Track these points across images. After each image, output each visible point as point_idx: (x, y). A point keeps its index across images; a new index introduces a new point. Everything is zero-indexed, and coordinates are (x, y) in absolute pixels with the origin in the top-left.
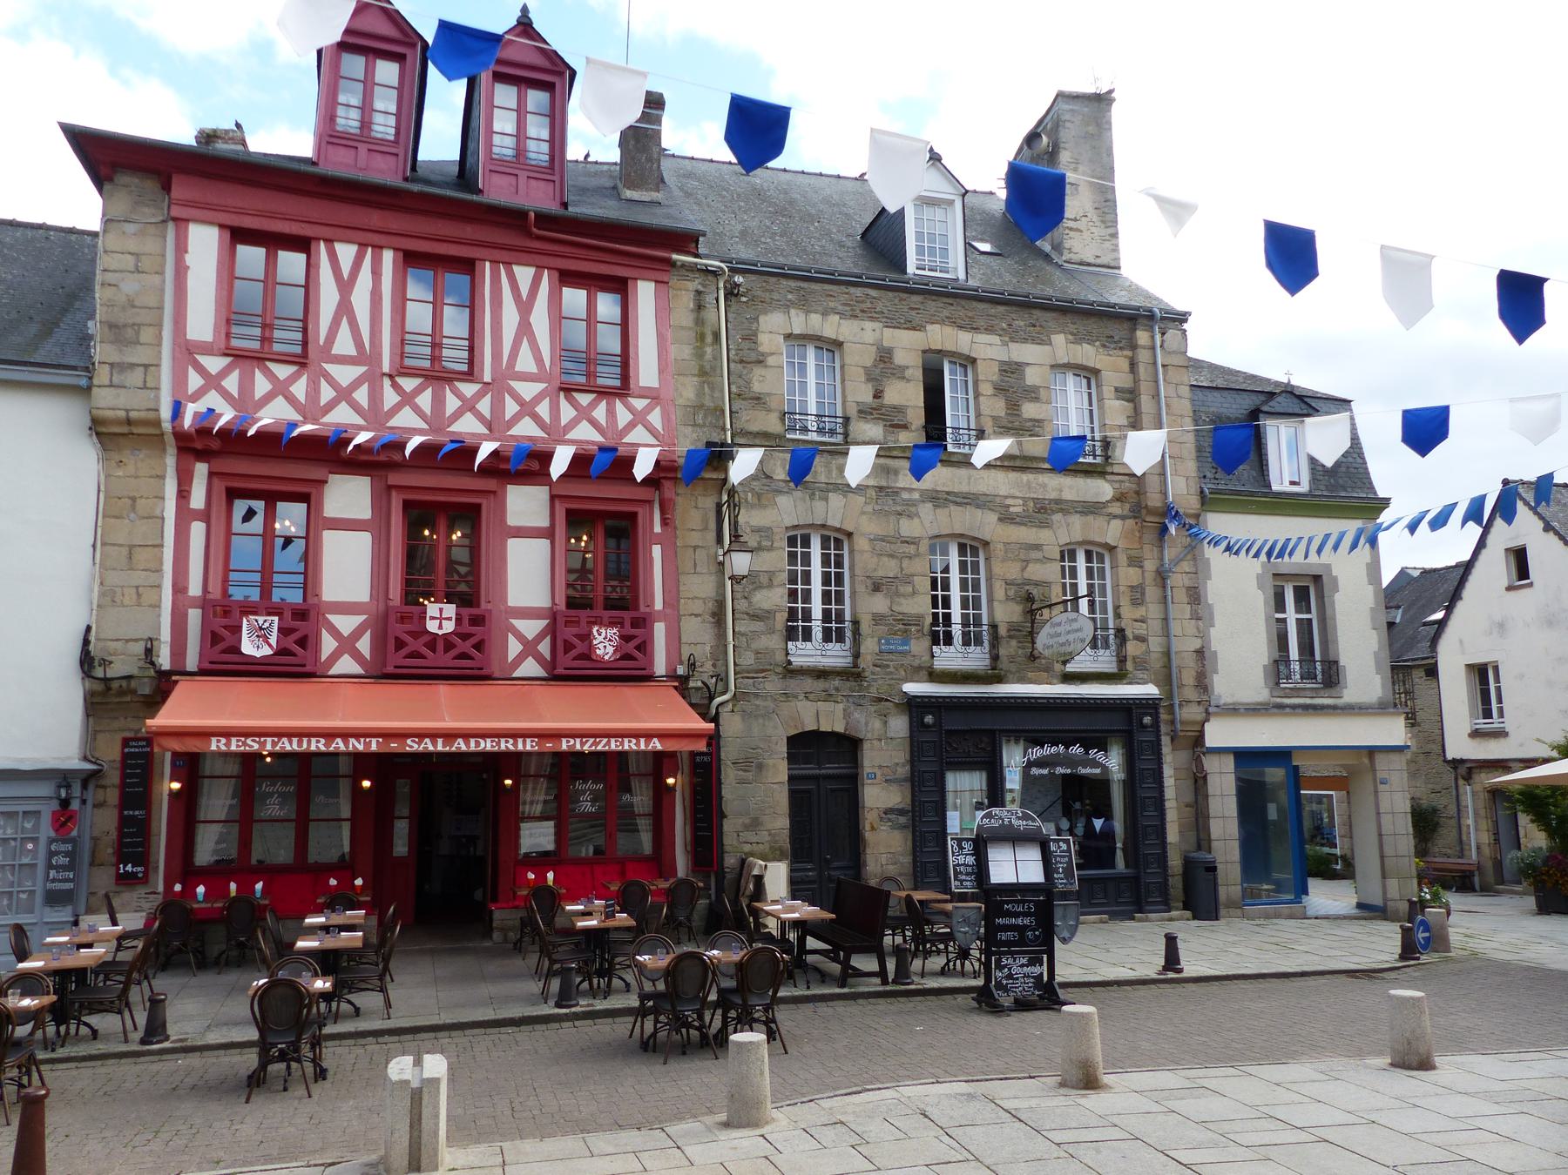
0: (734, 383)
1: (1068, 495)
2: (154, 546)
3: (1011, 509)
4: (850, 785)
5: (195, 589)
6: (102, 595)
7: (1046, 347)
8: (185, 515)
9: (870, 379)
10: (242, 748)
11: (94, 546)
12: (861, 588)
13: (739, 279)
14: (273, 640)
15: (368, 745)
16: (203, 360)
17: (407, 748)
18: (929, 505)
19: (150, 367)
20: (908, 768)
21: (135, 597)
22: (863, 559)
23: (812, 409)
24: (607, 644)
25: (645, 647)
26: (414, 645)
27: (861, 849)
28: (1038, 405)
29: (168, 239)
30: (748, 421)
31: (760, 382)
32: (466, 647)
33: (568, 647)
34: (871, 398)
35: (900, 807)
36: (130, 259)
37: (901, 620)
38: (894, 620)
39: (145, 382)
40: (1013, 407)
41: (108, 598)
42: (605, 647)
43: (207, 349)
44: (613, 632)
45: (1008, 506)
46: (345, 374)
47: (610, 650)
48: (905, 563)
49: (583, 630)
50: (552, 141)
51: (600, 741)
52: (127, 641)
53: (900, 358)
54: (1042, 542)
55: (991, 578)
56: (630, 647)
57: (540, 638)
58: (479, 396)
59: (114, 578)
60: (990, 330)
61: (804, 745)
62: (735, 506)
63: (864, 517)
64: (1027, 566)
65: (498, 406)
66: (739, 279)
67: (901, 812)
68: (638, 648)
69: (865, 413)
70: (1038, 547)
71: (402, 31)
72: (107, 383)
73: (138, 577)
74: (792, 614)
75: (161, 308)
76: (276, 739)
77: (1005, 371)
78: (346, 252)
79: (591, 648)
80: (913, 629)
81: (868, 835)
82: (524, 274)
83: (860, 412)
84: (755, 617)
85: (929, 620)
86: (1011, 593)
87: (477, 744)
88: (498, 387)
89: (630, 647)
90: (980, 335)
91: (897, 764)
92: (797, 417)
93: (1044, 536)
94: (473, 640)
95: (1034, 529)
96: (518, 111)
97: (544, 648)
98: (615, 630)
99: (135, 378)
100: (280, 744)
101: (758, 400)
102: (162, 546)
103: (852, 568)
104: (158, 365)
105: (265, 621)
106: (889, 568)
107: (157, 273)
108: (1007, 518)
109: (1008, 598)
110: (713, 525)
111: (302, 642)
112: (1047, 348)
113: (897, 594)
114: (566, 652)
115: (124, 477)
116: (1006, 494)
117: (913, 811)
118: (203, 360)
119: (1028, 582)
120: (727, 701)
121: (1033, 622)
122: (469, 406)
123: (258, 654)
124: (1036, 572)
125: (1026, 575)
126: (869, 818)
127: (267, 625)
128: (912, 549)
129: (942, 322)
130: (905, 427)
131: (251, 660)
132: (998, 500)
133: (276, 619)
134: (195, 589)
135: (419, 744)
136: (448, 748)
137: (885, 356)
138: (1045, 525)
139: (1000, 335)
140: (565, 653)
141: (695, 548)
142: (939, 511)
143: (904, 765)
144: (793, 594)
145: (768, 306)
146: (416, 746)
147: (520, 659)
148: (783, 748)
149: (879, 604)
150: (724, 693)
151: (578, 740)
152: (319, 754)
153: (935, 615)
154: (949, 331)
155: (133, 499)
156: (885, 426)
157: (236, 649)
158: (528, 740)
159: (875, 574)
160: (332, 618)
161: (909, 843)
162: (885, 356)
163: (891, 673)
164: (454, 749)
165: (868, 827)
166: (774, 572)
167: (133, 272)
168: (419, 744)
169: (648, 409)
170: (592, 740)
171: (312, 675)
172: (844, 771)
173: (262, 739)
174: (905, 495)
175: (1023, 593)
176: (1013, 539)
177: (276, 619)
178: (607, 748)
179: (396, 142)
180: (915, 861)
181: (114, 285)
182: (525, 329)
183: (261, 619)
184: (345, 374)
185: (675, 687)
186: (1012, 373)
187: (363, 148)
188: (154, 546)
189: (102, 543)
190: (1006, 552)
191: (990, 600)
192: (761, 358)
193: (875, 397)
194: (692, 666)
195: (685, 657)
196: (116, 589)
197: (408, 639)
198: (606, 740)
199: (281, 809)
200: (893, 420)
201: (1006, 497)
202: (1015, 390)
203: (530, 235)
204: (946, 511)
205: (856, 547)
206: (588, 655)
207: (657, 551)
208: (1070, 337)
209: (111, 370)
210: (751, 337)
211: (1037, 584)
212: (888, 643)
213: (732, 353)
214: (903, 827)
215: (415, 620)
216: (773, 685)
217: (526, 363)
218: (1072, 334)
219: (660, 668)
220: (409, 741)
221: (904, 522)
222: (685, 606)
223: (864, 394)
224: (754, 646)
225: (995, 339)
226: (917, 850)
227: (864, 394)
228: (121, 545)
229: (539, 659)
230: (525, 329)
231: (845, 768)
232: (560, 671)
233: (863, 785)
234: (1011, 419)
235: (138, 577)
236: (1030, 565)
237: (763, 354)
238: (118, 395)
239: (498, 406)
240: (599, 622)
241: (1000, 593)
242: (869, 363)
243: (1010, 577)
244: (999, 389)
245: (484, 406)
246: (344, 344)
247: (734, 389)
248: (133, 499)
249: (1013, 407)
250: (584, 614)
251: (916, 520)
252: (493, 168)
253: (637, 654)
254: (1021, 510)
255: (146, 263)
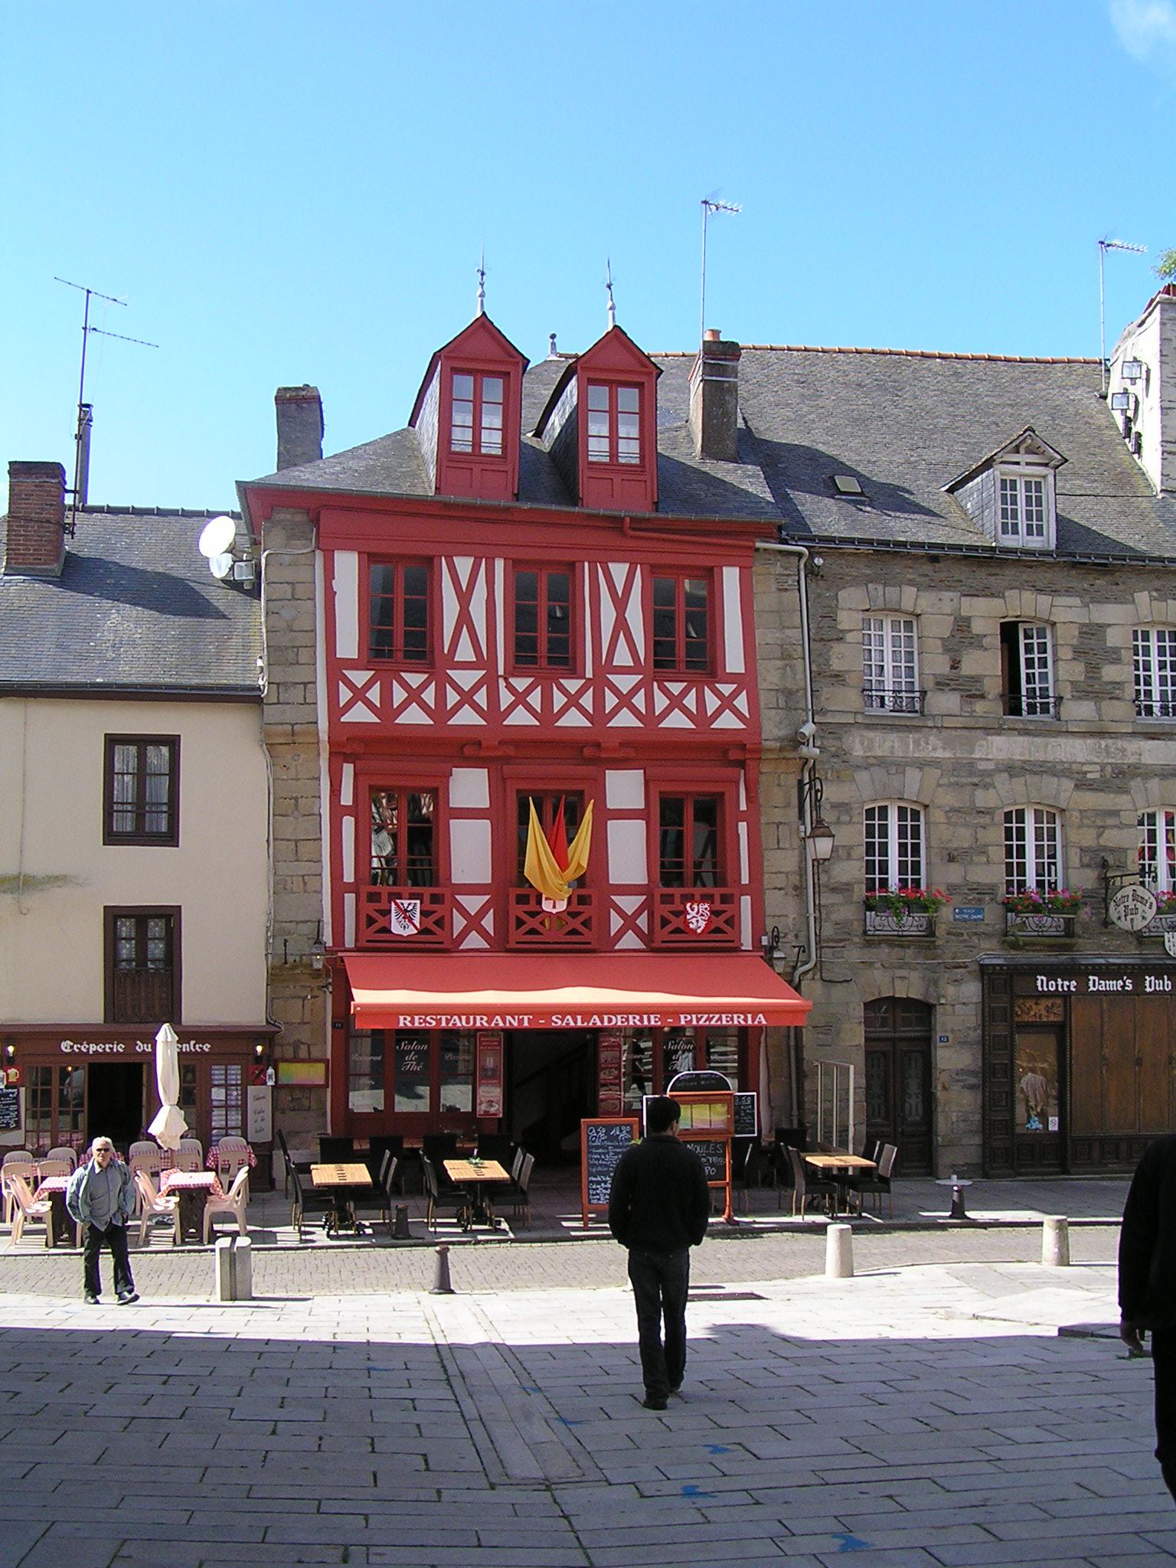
0: (814, 661)
1: (1147, 759)
2: (315, 840)
3: (1089, 776)
4: (925, 1047)
5: (349, 876)
6: (276, 883)
7: (1129, 606)
8: (338, 812)
9: (947, 650)
10: (423, 1025)
11: (268, 841)
12: (935, 860)
13: (819, 561)
14: (417, 922)
15: (521, 1021)
16: (350, 674)
17: (553, 1024)
18: (1005, 775)
19: (309, 684)
20: (979, 1031)
21: (302, 885)
22: (935, 833)
23: (889, 685)
24: (699, 918)
25: (733, 921)
26: (532, 923)
27: (934, 1106)
28: (1119, 666)
29: (316, 567)
30: (827, 699)
31: (841, 658)
32: (576, 923)
33: (665, 922)
34: (948, 669)
35: (972, 1068)
36: (288, 588)
37: (976, 889)
38: (968, 889)
39: (305, 698)
40: (1093, 670)
41: (280, 888)
42: (697, 921)
43: (352, 664)
44: (704, 907)
45: (1086, 773)
46: (467, 679)
47: (702, 924)
48: (980, 832)
49: (679, 907)
50: (642, 439)
51: (713, 1017)
52: (298, 923)
53: (977, 627)
54: (1118, 807)
55: (1066, 846)
56: (719, 922)
57: (638, 913)
58: (581, 692)
59: (285, 869)
60: (1069, 592)
61: (881, 1009)
62: (817, 791)
63: (940, 790)
64: (1103, 832)
65: (599, 701)
66: (819, 561)
67: (972, 1073)
68: (726, 922)
69: (941, 684)
70: (1115, 813)
71: (503, 347)
72: (276, 701)
73: (304, 868)
74: (870, 885)
75: (314, 631)
76: (449, 1017)
77: (1084, 633)
78: (464, 565)
79: (686, 923)
80: (987, 898)
81: (940, 1094)
82: (619, 571)
83: (938, 684)
84: (834, 890)
85: (1003, 888)
86: (1086, 860)
87: (610, 1020)
88: (599, 683)
89: (719, 922)
90: (1060, 598)
91: (969, 1028)
92: (874, 693)
93: (1122, 801)
94: (582, 918)
95: (1112, 796)
96: (610, 412)
97: (642, 922)
98: (706, 906)
99: (297, 694)
100: (452, 1022)
101: (838, 678)
102: (320, 839)
103: (927, 840)
104: (314, 683)
105: (409, 904)
106: (963, 838)
107: (309, 599)
108: (1083, 784)
109: (1083, 866)
110: (795, 802)
111: (439, 923)
112: (1130, 607)
113: (971, 862)
114: (662, 927)
115: (288, 780)
116: (1083, 761)
117: (984, 1072)
118: (350, 674)
119: (1105, 849)
120: (810, 970)
121: (1107, 888)
122: (573, 701)
123: (405, 933)
124: (1112, 838)
125: (1102, 842)
126: (940, 1079)
127: (411, 907)
128: (985, 820)
129: (1020, 588)
130: (982, 697)
131: (400, 939)
132: (1074, 766)
133: (418, 902)
134: (349, 876)
135: (562, 1021)
136: (586, 1024)
137: (962, 625)
138: (1124, 790)
139: (1081, 597)
140: (662, 927)
141: (779, 824)
142: (1014, 780)
143: (975, 1030)
144: (870, 867)
145: (842, 582)
146: (560, 1022)
147: (621, 933)
148: (860, 1012)
149: (954, 874)
150: (807, 963)
151: (694, 1016)
152: (482, 1029)
153: (1010, 883)
154: (1028, 596)
155: (296, 799)
156: (962, 696)
157: (387, 930)
158: (652, 1017)
159: (950, 845)
160: (461, 898)
161: (979, 1102)
162: (962, 625)
163: (965, 941)
164: (591, 1024)
165: (939, 1087)
166: (852, 847)
167: (290, 600)
168: (562, 1021)
169: (735, 694)
170: (706, 1016)
171: (447, 951)
172: (917, 1034)
173: (439, 1017)
174: (982, 766)
175: (1098, 860)
176: (1090, 806)
177: (418, 902)
178: (719, 1023)
179: (504, 456)
180: (983, 1118)
181: (277, 613)
182: (621, 624)
183: (406, 902)
184: (467, 679)
185: (762, 957)
186: (1092, 634)
187: (477, 469)
188: (315, 840)
189: (275, 839)
190: (1081, 819)
191: (1066, 868)
192: (841, 636)
193: (953, 667)
194: (776, 938)
195: (769, 929)
196: (287, 878)
197: (671, 917)
198: (717, 1016)
199: (418, 1065)
200: (972, 691)
201: (1083, 764)
202: (1095, 652)
203: (625, 535)
204: (1022, 779)
205: (932, 819)
206: (684, 929)
207: (743, 827)
208: (1154, 594)
209: (278, 688)
210: (831, 616)
211: (1112, 850)
212: (961, 912)
213: (813, 631)
214: (971, 1087)
215: (533, 901)
216: (854, 954)
217: (623, 658)
218: (1156, 590)
219: (747, 943)
220: (554, 1018)
221: (979, 792)
222: (768, 880)
223: (940, 665)
224: (834, 917)
225: (1077, 601)
226: (987, 1107)
227: (940, 665)
228: (288, 840)
229: (638, 932)
230: (621, 624)
231: (917, 1031)
232: (657, 944)
233: (935, 1048)
234: (1090, 682)
235: (304, 868)
236: (1107, 831)
237: (842, 631)
238: (284, 712)
239: (599, 701)
240: (691, 898)
241: (1075, 860)
242: (947, 634)
243: (1084, 844)
244: (1079, 653)
245: (587, 701)
246: (465, 652)
247: (814, 668)
248: (296, 799)
249: (1093, 670)
250: (677, 891)
251: (991, 790)
252: (591, 474)
253: (727, 928)
254: (1099, 777)
255: (301, 591)
